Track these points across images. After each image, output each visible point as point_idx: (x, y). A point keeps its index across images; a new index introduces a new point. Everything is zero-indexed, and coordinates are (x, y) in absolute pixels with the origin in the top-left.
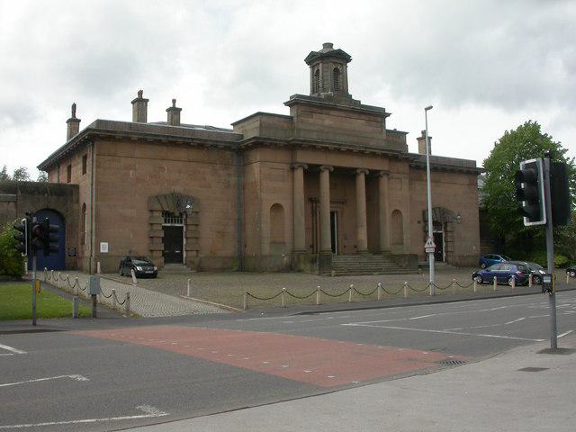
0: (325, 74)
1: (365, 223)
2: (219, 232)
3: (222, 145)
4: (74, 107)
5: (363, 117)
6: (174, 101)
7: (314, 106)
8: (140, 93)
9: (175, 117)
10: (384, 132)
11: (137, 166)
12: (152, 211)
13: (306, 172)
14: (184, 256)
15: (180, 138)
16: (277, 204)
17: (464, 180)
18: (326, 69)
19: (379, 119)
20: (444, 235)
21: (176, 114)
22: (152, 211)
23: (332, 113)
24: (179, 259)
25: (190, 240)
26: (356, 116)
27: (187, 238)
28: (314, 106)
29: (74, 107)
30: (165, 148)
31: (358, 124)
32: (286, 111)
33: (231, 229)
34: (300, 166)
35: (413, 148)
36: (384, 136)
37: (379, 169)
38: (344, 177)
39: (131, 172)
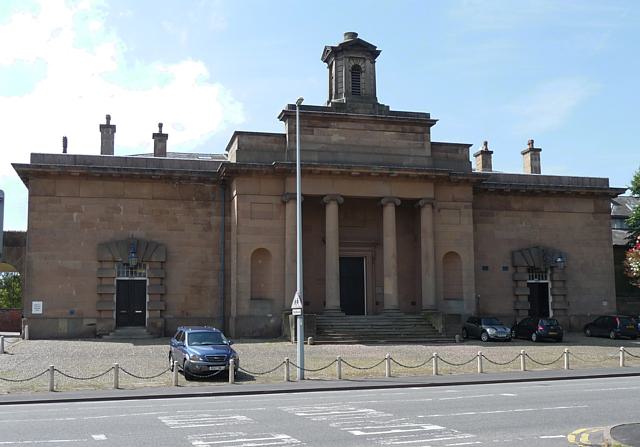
0: (339, 69)
1: (393, 271)
2: (193, 286)
3: (76, 172)
4: (65, 140)
5: (393, 127)
6: (161, 126)
7: (314, 118)
8: (108, 118)
9: (160, 145)
10: (428, 145)
11: (83, 207)
12: (101, 261)
13: (397, 208)
14: (147, 316)
15: (136, 170)
16: (259, 250)
17: (588, 206)
18: (345, 65)
19: (420, 129)
20: (550, 286)
21: (160, 141)
22: (101, 261)
23: (342, 125)
24: (140, 321)
25: (558, 299)
26: (382, 126)
27: (553, 295)
28: (314, 118)
29: (65, 140)
30: (101, 183)
31: (388, 137)
32: (282, 128)
33: (212, 282)
34: (428, 203)
35: (477, 165)
36: (428, 152)
37: (419, 197)
38: (360, 212)
39: (75, 215)
